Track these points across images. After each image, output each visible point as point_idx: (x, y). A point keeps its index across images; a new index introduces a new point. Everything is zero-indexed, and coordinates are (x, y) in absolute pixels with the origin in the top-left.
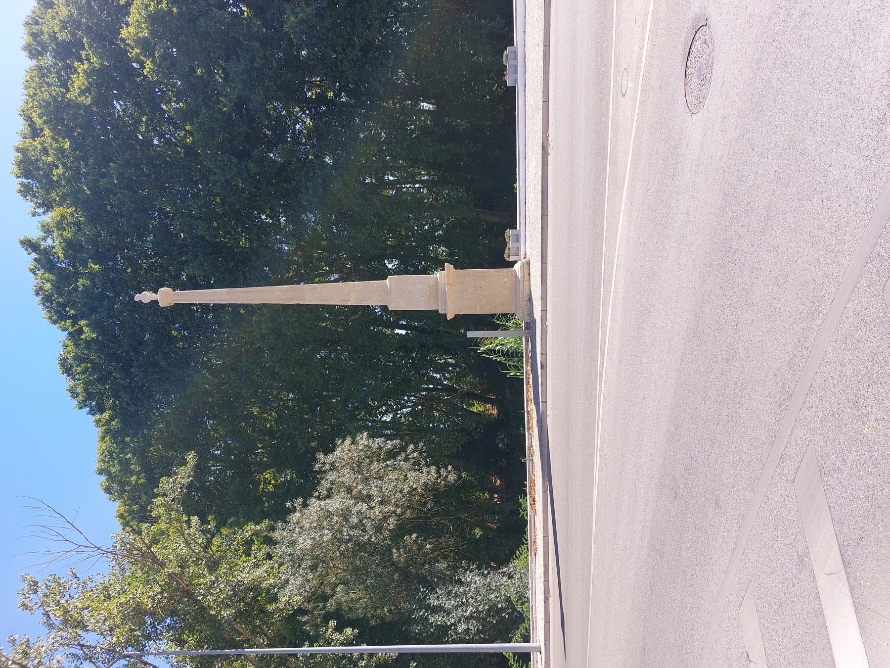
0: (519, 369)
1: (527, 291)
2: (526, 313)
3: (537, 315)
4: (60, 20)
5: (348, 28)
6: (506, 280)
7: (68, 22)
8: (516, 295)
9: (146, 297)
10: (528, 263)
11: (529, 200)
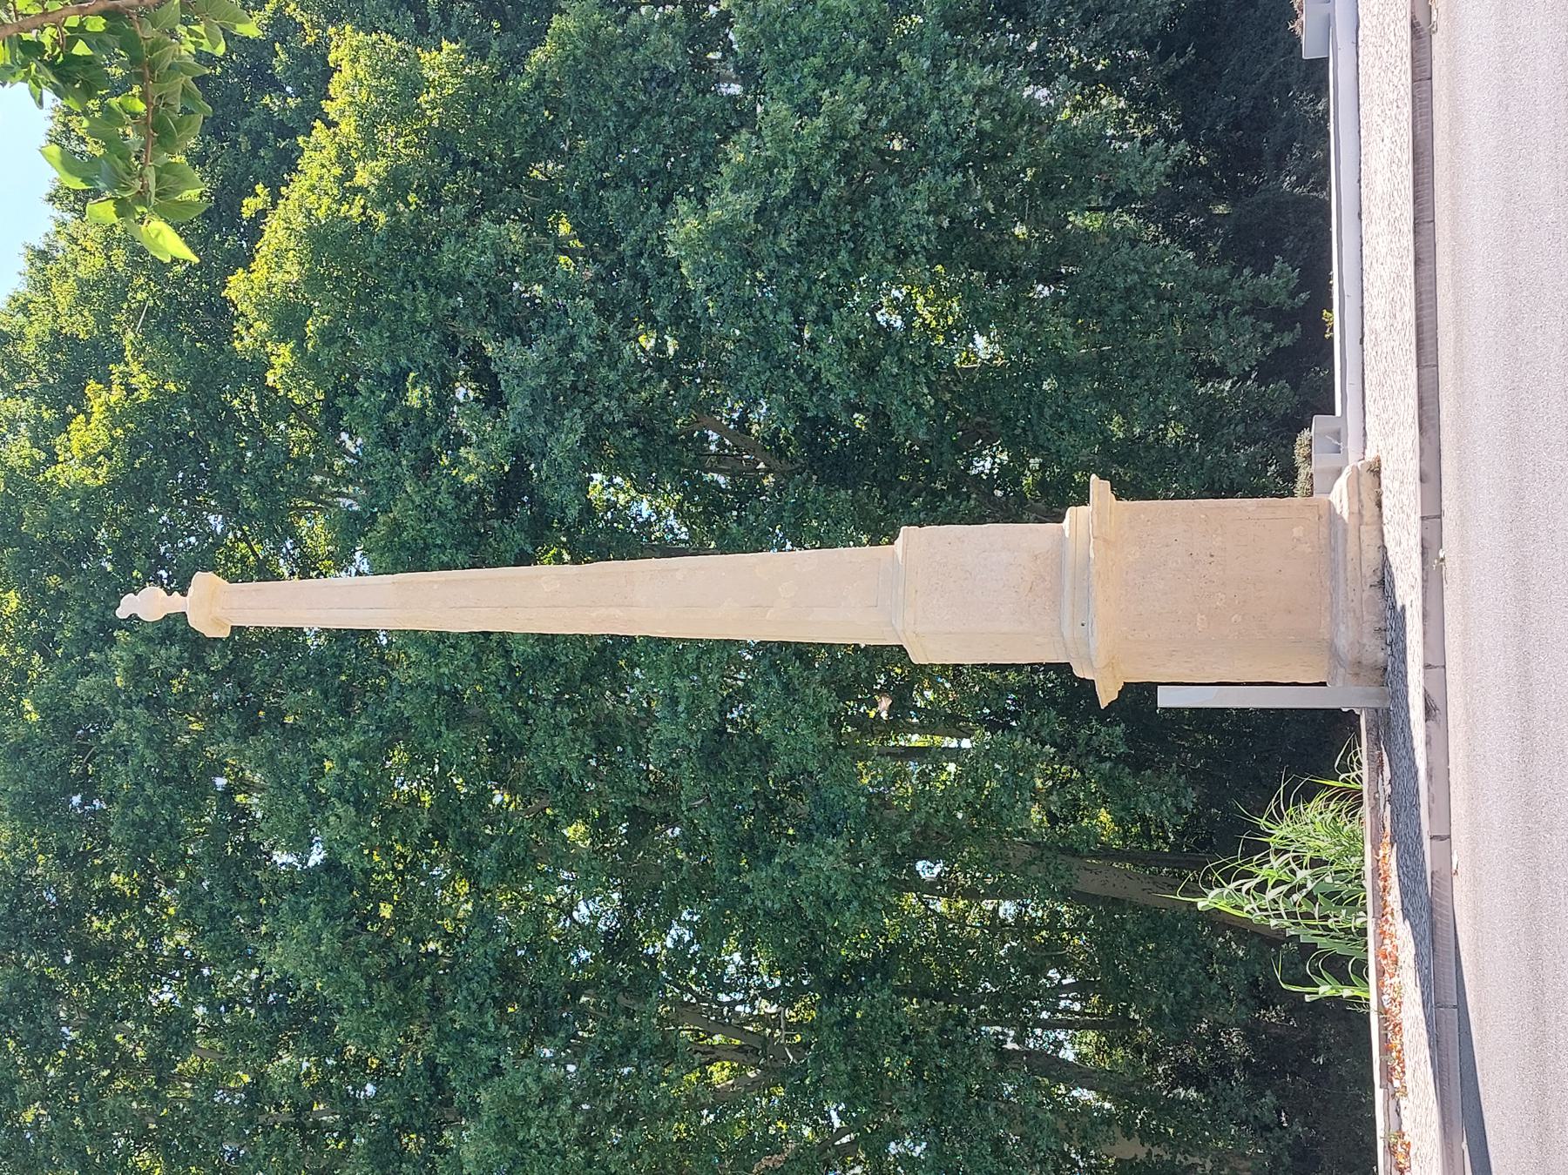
0: (1347, 968)
1: (1371, 557)
2: (1368, 629)
3: (1408, 592)
4: (78, 280)
5: (843, 256)
6: (1297, 532)
7: (95, 286)
8: (1334, 577)
9: (148, 604)
10: (1376, 471)
11: (1373, 209)
